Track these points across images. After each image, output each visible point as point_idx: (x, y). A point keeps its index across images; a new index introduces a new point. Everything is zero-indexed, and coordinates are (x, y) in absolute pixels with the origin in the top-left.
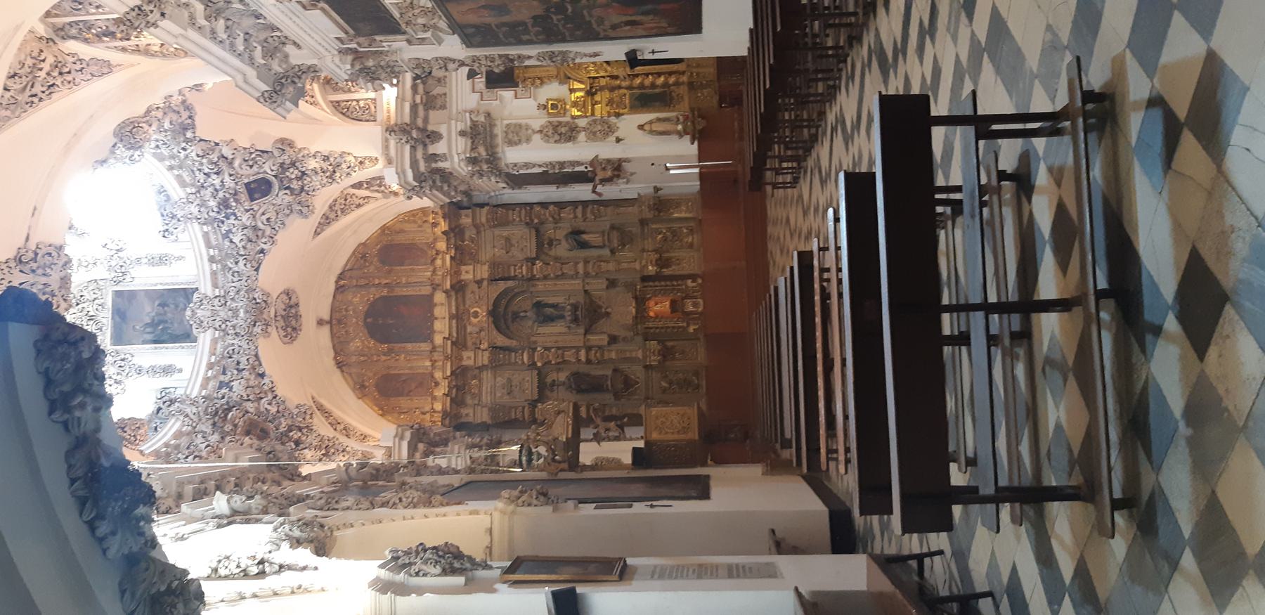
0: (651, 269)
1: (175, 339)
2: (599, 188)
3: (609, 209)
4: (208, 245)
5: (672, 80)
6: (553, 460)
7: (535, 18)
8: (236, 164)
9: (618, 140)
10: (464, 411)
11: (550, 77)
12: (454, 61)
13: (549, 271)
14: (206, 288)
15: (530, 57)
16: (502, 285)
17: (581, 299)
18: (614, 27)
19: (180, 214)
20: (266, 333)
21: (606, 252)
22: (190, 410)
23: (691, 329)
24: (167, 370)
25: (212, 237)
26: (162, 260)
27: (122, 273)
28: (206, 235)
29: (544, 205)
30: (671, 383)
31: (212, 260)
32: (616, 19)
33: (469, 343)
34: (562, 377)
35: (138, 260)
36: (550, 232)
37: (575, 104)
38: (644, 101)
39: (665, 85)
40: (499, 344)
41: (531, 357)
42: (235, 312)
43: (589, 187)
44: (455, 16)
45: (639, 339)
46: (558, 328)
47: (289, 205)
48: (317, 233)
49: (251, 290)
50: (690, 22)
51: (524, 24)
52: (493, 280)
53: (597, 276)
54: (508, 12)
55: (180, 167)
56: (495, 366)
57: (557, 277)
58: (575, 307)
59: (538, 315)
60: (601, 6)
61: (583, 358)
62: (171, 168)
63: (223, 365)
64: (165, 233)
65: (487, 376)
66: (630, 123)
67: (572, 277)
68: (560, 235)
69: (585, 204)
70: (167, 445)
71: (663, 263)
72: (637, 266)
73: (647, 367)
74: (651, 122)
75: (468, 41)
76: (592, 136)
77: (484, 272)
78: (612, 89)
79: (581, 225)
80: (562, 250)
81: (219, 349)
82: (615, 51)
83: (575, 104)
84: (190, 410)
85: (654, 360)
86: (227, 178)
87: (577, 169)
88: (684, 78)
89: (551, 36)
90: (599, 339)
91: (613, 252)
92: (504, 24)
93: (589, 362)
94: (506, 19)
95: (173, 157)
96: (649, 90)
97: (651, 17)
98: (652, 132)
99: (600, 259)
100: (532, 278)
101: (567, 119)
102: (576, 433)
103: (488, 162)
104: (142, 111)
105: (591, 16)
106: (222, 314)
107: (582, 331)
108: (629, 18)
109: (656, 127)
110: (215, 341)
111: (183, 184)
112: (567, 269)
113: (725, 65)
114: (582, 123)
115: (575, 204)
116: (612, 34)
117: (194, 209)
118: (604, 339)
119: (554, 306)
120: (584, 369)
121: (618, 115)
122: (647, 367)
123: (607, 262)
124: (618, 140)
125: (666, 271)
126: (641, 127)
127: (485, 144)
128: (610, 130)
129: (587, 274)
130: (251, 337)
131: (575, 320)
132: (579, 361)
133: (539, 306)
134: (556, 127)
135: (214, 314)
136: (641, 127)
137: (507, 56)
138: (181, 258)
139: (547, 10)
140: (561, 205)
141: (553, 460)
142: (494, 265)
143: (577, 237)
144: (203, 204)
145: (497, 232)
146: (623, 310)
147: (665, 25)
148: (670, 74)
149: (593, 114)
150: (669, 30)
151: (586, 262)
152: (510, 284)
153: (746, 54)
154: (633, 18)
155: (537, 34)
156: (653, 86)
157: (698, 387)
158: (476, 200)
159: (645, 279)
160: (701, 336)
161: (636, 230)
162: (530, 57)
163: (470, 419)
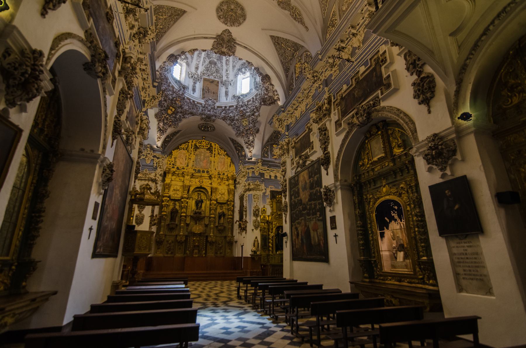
0: (209, 239)
1: (203, 94)
2: (238, 223)
3: (230, 226)
4: (230, 107)
5: (270, 249)
6: (137, 194)
7: (301, 200)
8: (253, 117)
9: (253, 230)
10: (170, 175)
11: (273, 210)
12: (285, 174)
13: (213, 206)
14: (217, 104)
15: (285, 199)
16: (209, 191)
17: (203, 215)
18: (297, 229)
19: (240, 100)
20: (202, 119)
21: (217, 224)
22: (181, 92)
23: (187, 252)
24: (194, 90)
25: (232, 108)
26: (227, 94)
27: (224, 84)
28: (233, 106)
29: (233, 206)
30: (170, 244)
31: (226, 107)
32: (300, 229)
33: (192, 179)
34: (177, 207)
35: (227, 88)
36: (225, 207)
37: (264, 217)
38: (265, 239)
39: (269, 247)
40: (191, 188)
41: (185, 198)
42: (210, 111)
43: (238, 219)
44: (302, 173)
45: (186, 233)
46: (194, 207)
47: (239, 130)
48: (230, 138)
49: (215, 116)
50: (295, 257)
51: (299, 196)
52: (211, 188)
53: (209, 221)
54: (303, 191)
55: (253, 101)
56: (184, 186)
57: (210, 208)
58: (200, 213)
59: (199, 201)
60: (305, 223)
61: (182, 214)
62: (253, 98)
63: (194, 104)
64: (234, 96)
65: (181, 184)
66: (257, 233)
67: (210, 213)
68: (224, 210)
69: (233, 219)
70: (170, 83)
71: (212, 243)
72: (211, 234)
73: (176, 236)
74: (258, 241)
75: (290, 179)
76: (255, 222)
77: (215, 185)
78: (268, 229)
79: (227, 217)
80: (219, 210)
81: (199, 105)
82: (287, 228)
83: (264, 217)
84: (181, 92)
85: (179, 238)
86: (249, 113)
87: (244, 216)
88: (271, 253)
89: (293, 206)
90: (188, 220)
91: (217, 227)
92: (298, 190)
93: (181, 216)
94: (301, 190)
95: (256, 99)
96: (272, 240)
97: (300, 242)
98: (255, 241)
99: (215, 222)
100: (211, 200)
101: (260, 214)
102: (186, 239)
103: (249, 188)
104: (273, 83)
105: (301, 220)
106: (209, 107)
107: (192, 215)
108: (300, 233)
109: (256, 243)
110: (201, 104)
111: (248, 101)
112: (212, 212)
113: (279, 268)
114: (259, 219)
115: (233, 216)
116: (293, 228)
117: (241, 104)
118: (188, 222)
119: (201, 206)
120: (179, 215)
121: (261, 230)
122: (176, 236)
123: (214, 225)
124: (253, 230)
125: (208, 245)
126: (256, 238)
127: (254, 188)
128: (256, 228)
129: (210, 218)
130: (201, 114)
131: (196, 213)
132: (182, 213)
133: (202, 201)
134: (258, 210)
135: (210, 105)
136: (256, 238)
137: (286, 191)
138: (227, 99)
139: (304, 204)
140: (233, 211)
141: (137, 194)
142: (216, 189)
143: (222, 215)
144: (242, 106)
145: (226, 191)
146: (197, 228)
147: (297, 246)
148: (272, 248)
149: (261, 222)
150: (295, 249)
151: (214, 218)
152: (210, 193)
153: (284, 277)
154: (300, 235)
155: (294, 201)
156: (269, 242)
157: (167, 253)
158: (237, 186)
159: (207, 237)
160: (185, 255)
161: (224, 235)
162: (285, 199)
163: (167, 176)
